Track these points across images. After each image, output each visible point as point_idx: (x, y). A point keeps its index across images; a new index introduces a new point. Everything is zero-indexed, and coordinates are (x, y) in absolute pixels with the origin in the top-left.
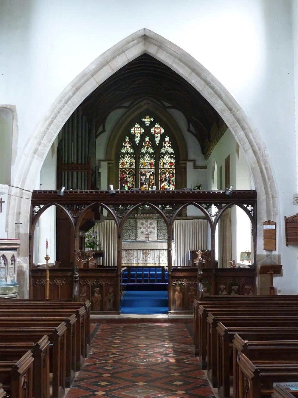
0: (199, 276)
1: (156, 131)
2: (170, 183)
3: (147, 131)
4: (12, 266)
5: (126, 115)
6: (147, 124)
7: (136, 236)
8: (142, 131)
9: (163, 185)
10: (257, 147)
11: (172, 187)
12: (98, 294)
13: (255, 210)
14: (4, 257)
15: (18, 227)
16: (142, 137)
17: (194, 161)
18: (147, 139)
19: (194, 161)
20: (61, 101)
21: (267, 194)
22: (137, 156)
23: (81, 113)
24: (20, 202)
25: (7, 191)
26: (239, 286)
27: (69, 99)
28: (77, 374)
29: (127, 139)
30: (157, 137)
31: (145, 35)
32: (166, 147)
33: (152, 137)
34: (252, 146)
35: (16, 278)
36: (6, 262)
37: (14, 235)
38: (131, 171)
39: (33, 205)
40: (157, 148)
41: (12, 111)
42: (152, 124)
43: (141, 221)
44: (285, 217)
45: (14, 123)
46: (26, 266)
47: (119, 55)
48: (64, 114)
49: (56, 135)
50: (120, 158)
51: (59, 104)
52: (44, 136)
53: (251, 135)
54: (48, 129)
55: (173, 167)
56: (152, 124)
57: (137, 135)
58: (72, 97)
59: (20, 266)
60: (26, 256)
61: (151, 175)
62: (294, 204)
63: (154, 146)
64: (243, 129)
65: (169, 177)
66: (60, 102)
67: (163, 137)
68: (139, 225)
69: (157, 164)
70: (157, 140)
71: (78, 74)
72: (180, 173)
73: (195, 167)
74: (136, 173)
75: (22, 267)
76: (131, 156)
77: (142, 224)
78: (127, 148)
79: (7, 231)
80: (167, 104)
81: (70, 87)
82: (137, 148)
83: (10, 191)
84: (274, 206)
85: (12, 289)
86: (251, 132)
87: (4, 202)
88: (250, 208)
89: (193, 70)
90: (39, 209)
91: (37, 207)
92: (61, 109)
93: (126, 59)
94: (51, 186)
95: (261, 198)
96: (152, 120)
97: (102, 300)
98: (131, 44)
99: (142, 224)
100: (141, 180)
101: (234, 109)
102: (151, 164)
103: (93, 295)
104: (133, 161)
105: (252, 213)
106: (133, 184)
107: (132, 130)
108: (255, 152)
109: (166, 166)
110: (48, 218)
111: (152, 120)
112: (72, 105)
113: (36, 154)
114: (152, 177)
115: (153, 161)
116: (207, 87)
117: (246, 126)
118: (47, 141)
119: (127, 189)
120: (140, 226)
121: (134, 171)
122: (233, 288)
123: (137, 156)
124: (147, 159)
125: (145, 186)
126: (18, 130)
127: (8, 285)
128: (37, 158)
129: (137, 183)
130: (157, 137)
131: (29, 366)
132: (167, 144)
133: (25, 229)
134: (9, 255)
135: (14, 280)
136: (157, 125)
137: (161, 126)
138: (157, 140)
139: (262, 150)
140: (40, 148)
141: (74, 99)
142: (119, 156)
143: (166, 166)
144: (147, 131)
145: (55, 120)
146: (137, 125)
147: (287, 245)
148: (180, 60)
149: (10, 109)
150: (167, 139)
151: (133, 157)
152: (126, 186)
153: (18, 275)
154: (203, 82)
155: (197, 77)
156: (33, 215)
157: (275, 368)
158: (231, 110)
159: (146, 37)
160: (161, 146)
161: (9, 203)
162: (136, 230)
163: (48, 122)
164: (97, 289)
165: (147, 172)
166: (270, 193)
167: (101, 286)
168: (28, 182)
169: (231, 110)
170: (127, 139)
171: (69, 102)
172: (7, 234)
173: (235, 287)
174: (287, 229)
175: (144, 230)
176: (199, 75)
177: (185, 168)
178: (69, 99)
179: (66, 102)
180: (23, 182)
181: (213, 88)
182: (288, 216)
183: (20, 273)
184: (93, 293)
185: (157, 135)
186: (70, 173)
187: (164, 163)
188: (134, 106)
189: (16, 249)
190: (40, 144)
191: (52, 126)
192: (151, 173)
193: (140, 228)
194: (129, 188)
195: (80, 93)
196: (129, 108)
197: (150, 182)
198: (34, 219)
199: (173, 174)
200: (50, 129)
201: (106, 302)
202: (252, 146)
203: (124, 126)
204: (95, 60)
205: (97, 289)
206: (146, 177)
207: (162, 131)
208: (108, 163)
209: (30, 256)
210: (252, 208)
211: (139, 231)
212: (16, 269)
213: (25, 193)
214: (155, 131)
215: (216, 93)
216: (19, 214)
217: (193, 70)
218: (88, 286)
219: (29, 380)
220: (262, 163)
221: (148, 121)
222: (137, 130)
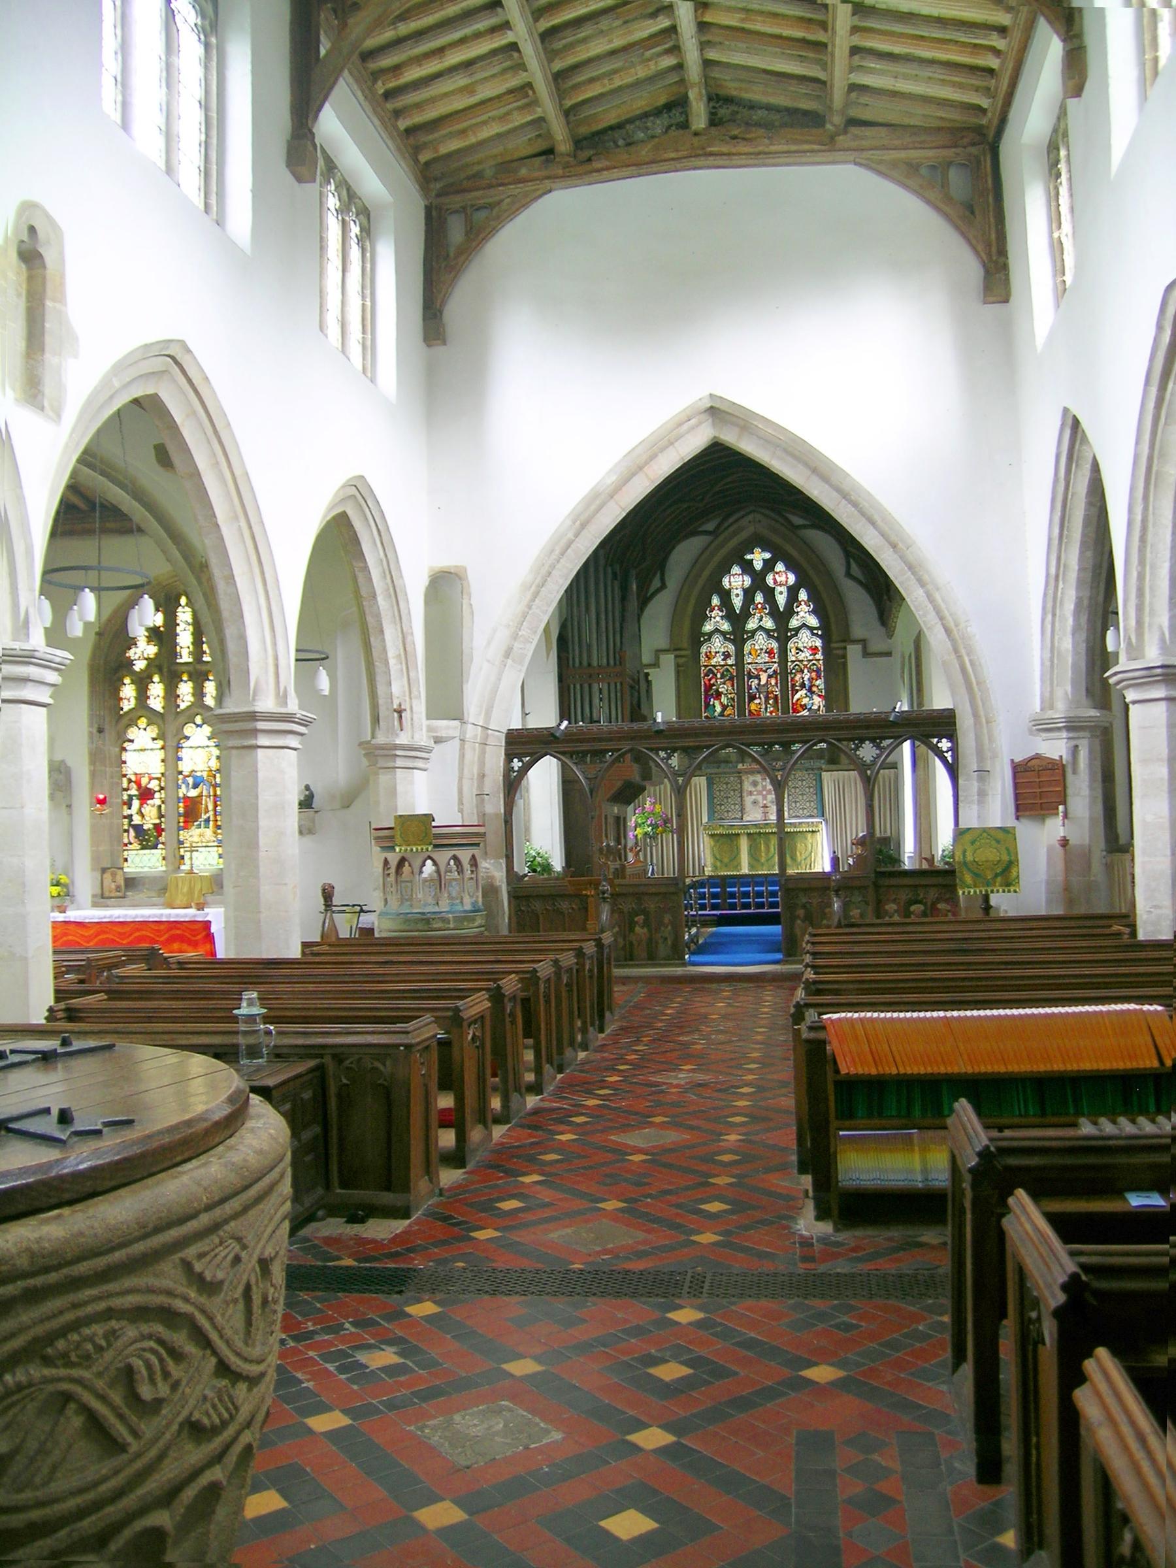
0: (833, 884)
1: (778, 579)
2: (813, 693)
3: (759, 581)
5: (707, 553)
6: (758, 565)
7: (742, 810)
8: (748, 581)
9: (797, 696)
10: (950, 619)
11: (817, 702)
12: (642, 927)
13: (954, 750)
14: (455, 858)
16: (749, 594)
17: (863, 642)
18: (759, 598)
19: (863, 642)
20: (552, 551)
21: (976, 715)
22: (739, 636)
23: (602, 562)
24: (483, 752)
25: (457, 733)
26: (925, 904)
27: (568, 546)
28: (582, 1055)
29: (716, 601)
30: (781, 593)
31: (712, 407)
32: (802, 614)
33: (770, 594)
34: (942, 619)
35: (480, 899)
36: (460, 870)
37: (475, 817)
38: (727, 670)
39: (509, 758)
40: (782, 617)
41: (460, 579)
42: (769, 566)
43: (751, 778)
44: (1012, 761)
45: (465, 602)
46: (499, 875)
47: (662, 450)
49: (555, 604)
50: (701, 644)
53: (937, 596)
54: (530, 607)
55: (819, 656)
56: (769, 566)
57: (736, 592)
59: (488, 877)
60: (501, 858)
61: (770, 677)
62: (1031, 733)
63: (775, 613)
64: (922, 583)
65: (811, 679)
67: (793, 593)
68: (747, 786)
69: (784, 652)
70: (781, 600)
71: (581, 497)
72: (834, 666)
73: (866, 654)
74: (739, 674)
75: (492, 877)
76: (726, 639)
77: (755, 784)
78: (716, 621)
79: (461, 811)
80: (797, 521)
81: (569, 522)
82: (738, 619)
83: (463, 732)
84: (991, 740)
85: (473, 920)
86: (938, 589)
88: (945, 744)
89: (815, 471)
90: (520, 764)
91: (516, 760)
92: (553, 567)
93: (678, 458)
94: (545, 715)
95: (965, 723)
96: (767, 556)
97: (650, 940)
98: (686, 427)
99: (755, 784)
100: (750, 687)
101: (900, 545)
102: (770, 652)
103: (632, 929)
104: (731, 648)
105: (948, 755)
106: (733, 699)
107: (726, 582)
108: (948, 631)
109: (801, 656)
110: (544, 779)
111: (767, 556)
114: (773, 682)
115: (775, 645)
116: (844, 502)
117: (926, 577)
119: (718, 709)
120: (751, 788)
121: (733, 670)
122: (912, 908)
123: (739, 636)
124: (761, 641)
125: (757, 701)
126: (472, 613)
127: (466, 911)
129: (744, 696)
130: (781, 593)
131: (196, 475)
132: (803, 607)
133: (495, 805)
134: (465, 855)
135: (476, 902)
136: (780, 567)
137: (789, 568)
138: (781, 600)
139: (962, 625)
140: (517, 645)
142: (698, 639)
143: (801, 656)
144: (759, 581)
146: (736, 570)
147: (1017, 818)
148: (785, 451)
149: (456, 574)
150: (803, 595)
151: (729, 640)
152: (717, 703)
153: (485, 895)
154: (835, 494)
155: (823, 484)
156: (509, 776)
158: (894, 546)
159: (716, 411)
160: (790, 612)
162: (741, 797)
163: (529, 595)
164: (640, 918)
165: (761, 670)
166: (982, 713)
167: (645, 912)
168: (495, 713)
169: (894, 546)
170: (716, 601)
173: (916, 908)
174: (1016, 785)
175: (760, 798)
176: (826, 479)
177: (844, 657)
178: (568, 546)
179: (563, 554)
181: (855, 505)
182: (1017, 760)
183: (490, 891)
184: (631, 926)
185: (778, 589)
186: (586, 686)
187: (797, 648)
188: (726, 529)
189: (477, 845)
192: (770, 672)
193: (751, 793)
194: (724, 707)
196: (714, 533)
197: (768, 693)
198: (513, 785)
199: (818, 671)
201: (657, 943)
202: (942, 619)
203: (706, 573)
204: (616, 465)
205: (640, 918)
206: (760, 680)
207: (792, 579)
208: (676, 657)
209: (507, 856)
210: (949, 745)
211: (748, 800)
212: (481, 882)
214: (775, 580)
215: (863, 514)
216: (482, 776)
217: (815, 471)
218: (621, 912)
219: (483, 1033)
220: (963, 652)
221: (758, 558)
222: (736, 581)
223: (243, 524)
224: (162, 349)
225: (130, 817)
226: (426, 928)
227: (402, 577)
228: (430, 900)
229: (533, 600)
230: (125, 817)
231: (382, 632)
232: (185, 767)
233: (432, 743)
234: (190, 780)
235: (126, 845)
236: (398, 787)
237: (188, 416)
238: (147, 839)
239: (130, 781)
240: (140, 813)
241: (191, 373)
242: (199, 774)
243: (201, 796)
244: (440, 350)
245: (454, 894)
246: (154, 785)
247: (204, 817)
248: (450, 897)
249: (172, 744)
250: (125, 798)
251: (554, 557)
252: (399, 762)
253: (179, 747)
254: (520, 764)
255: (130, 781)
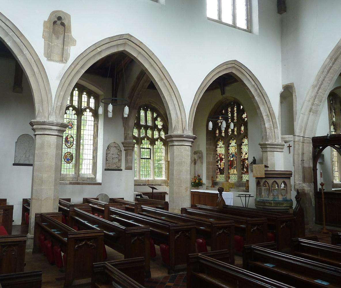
4: (285, 188)
15: (303, 162)
25: (292, 139)
27: (330, 69)
48: (329, 80)
51: (322, 74)
52: (315, 98)
58: (332, 66)
66: (323, 73)
79: (294, 166)
81: (328, 60)
83: (294, 139)
85: (283, 204)
87: (291, 146)
112: (333, 72)
113: (311, 112)
118: (318, 102)
128: (313, 115)
140: (313, 107)
141: (335, 68)
145: (322, 86)
157: (298, 259)
161: (294, 147)
163: (316, 89)
171: (331, 70)
172: (294, 168)
178: (330, 69)
179: (328, 72)
180: (304, 132)
190: (313, 105)
191: (320, 90)
195: (339, 62)
200: (319, 93)
213: (306, 139)
216: (303, 154)
223: (165, 81)
224: (120, 38)
225: (218, 165)
226: (263, 205)
227: (264, 90)
228: (267, 196)
229: (318, 90)
230: (217, 165)
231: (259, 108)
232: (230, 152)
233: (284, 143)
234: (231, 155)
235: (217, 173)
236: (268, 158)
237: (139, 54)
238: (222, 172)
239: (218, 156)
240: (220, 165)
241: (135, 42)
242: (233, 154)
243: (233, 160)
244: (285, 14)
245: (275, 194)
246: (223, 157)
247: (234, 166)
248: (273, 195)
249: (227, 146)
250: (217, 160)
251: (325, 73)
252: (268, 149)
253: (229, 146)
254: (319, 149)
255: (218, 156)
